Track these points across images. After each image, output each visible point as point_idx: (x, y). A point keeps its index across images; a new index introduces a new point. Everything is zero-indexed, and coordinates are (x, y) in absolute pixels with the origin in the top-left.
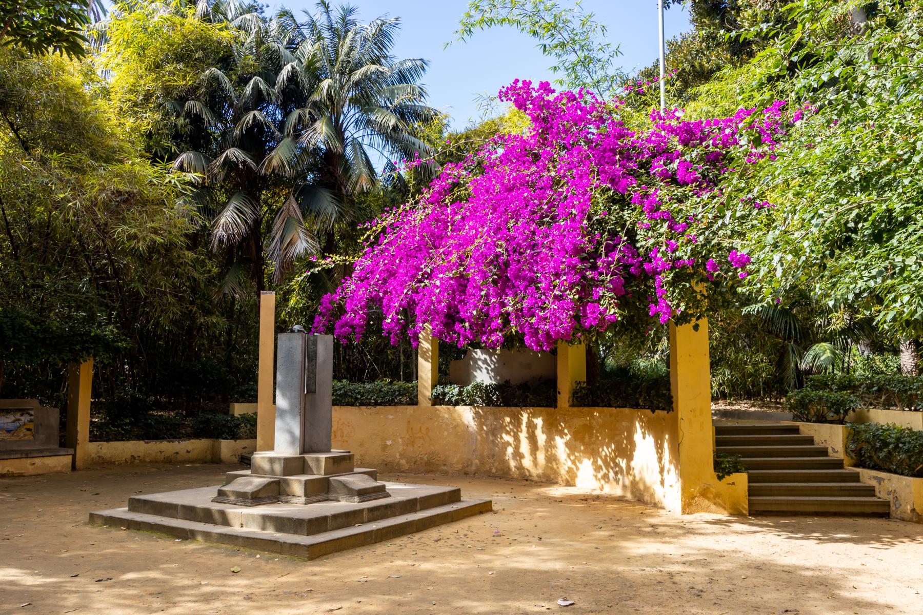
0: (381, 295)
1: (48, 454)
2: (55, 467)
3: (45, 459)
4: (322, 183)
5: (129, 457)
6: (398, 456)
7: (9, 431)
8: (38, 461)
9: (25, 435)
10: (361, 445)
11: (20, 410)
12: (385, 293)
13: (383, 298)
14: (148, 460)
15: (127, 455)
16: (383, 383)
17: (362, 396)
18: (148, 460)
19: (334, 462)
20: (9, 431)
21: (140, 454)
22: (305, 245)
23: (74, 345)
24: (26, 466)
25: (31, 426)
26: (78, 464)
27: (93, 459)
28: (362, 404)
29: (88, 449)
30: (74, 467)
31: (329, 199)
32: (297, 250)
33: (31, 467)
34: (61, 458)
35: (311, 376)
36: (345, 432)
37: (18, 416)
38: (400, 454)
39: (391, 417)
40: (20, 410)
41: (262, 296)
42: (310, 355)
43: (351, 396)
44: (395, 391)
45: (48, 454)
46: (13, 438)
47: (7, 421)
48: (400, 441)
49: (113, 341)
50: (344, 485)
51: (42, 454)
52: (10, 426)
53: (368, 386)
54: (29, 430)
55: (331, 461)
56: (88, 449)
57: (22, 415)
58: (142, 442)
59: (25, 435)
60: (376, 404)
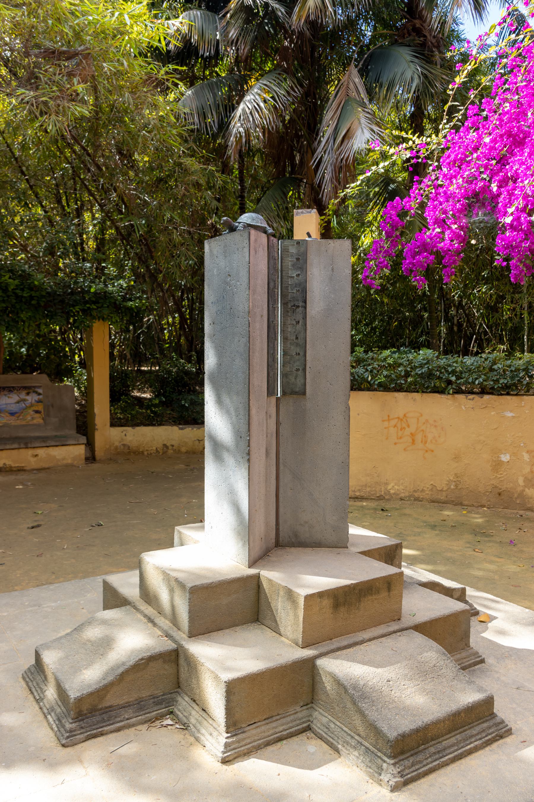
0: (494, 187)
1: (53, 443)
2: (64, 459)
3: (51, 449)
4: (399, 38)
5: (160, 446)
6: (521, 481)
7: (12, 414)
8: (41, 452)
9: (33, 418)
10: (457, 458)
11: (25, 388)
12: (502, 183)
13: (499, 195)
14: (183, 450)
15: (157, 444)
16: (496, 354)
17: (458, 378)
18: (183, 450)
19: (336, 606)
20: (12, 414)
21: (173, 443)
22: (367, 135)
23: (78, 305)
24: (27, 457)
25: (40, 407)
26: (99, 453)
27: (116, 448)
28: (458, 391)
29: (109, 435)
30: (91, 458)
31: (409, 58)
32: (355, 147)
33: (33, 460)
34: (71, 448)
35: (294, 350)
36: (430, 437)
37: (23, 395)
38: (526, 480)
39: (509, 414)
40: (25, 388)
41: (296, 219)
42: (288, 297)
43: (439, 378)
44: (517, 370)
45: (53, 443)
46: (19, 422)
47: (9, 401)
48: (526, 457)
49: (124, 299)
50: (353, 696)
51: (46, 441)
52: (14, 408)
53: (469, 360)
54: (37, 412)
55: (327, 602)
56: (109, 435)
57: (28, 394)
58: (175, 428)
59: (33, 418)
60: (483, 392)
